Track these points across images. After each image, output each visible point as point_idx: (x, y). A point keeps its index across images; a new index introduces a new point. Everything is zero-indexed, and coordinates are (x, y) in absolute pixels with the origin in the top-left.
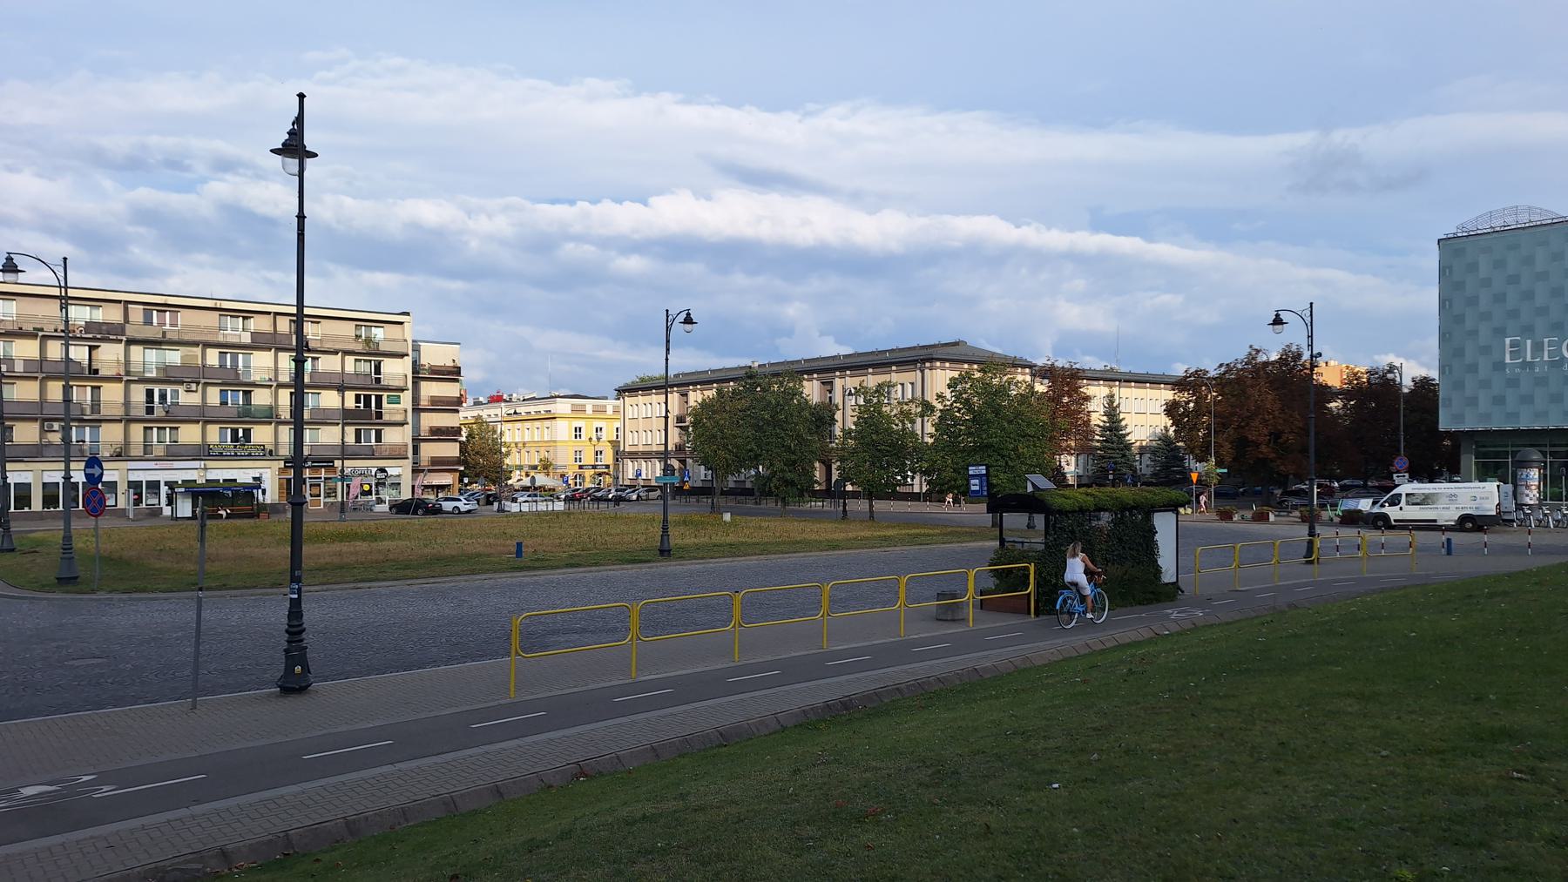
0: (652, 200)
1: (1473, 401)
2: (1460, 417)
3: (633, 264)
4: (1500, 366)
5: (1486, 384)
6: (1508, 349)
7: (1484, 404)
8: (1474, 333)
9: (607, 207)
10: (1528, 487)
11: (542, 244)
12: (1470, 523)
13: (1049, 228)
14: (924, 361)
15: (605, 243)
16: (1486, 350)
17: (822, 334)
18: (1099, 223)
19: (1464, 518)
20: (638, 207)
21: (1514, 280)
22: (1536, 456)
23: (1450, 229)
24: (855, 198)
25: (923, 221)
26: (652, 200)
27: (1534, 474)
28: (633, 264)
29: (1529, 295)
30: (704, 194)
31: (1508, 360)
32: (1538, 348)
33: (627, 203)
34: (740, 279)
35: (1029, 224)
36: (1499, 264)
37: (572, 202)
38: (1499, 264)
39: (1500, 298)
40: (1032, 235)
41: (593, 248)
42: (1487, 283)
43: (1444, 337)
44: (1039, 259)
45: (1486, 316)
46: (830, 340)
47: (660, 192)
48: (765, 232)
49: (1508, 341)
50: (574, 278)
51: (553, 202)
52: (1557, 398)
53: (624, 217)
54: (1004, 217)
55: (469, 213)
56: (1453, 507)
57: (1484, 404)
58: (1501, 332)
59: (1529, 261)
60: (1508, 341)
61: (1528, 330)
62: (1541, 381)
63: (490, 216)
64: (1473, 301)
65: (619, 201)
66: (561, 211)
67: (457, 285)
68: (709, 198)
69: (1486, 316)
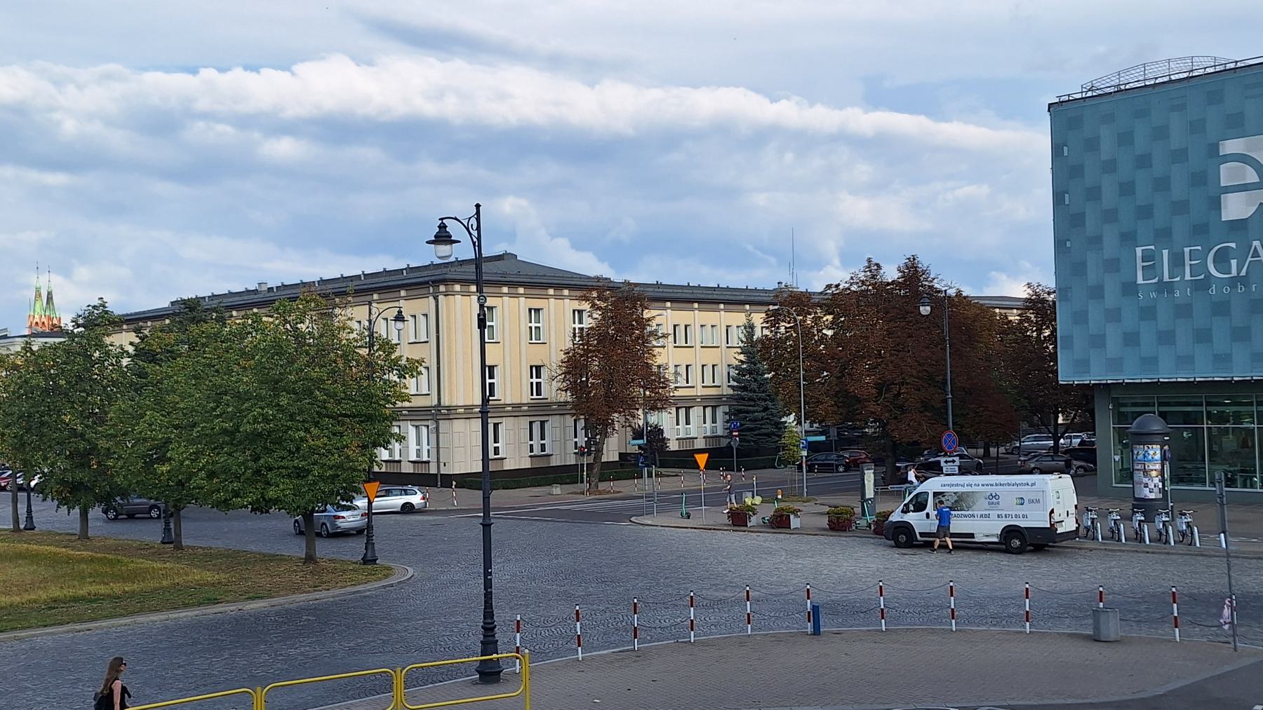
0: (297, 68)
1: (1098, 341)
2: (1083, 365)
3: (284, 148)
4: (1130, 288)
5: (1114, 315)
6: (1140, 264)
7: (1113, 344)
8: (1097, 241)
9: (238, 76)
10: (1146, 473)
11: (161, 123)
12: (1024, 541)
13: (811, 105)
14: (436, 283)
15: (245, 122)
16: (1112, 265)
17: (553, 236)
18: (877, 96)
19: (1010, 532)
20: (283, 76)
21: (1143, 161)
22: (1157, 426)
23: (1073, 87)
24: (555, 63)
25: (656, 93)
26: (295, 68)
27: (1155, 452)
28: (284, 148)
29: (1162, 184)
30: (363, 59)
31: (1140, 281)
32: (1177, 261)
33: (264, 71)
34: (430, 168)
35: (788, 98)
36: (1125, 139)
37: (193, 71)
38: (1125, 139)
39: (1127, 189)
40: (787, 112)
41: (229, 129)
42: (1110, 166)
43: (1060, 244)
44: (803, 141)
45: (1111, 216)
46: (563, 243)
47: (305, 57)
48: (450, 108)
49: (1139, 251)
50: (205, 169)
51: (167, 69)
52: (1241, 335)
53: (265, 89)
54: (757, 90)
55: (58, 83)
56: (994, 514)
57: (1113, 344)
58: (1129, 239)
59: (1161, 133)
60: (1139, 251)
61: (1163, 236)
62: (1183, 311)
63: (80, 87)
64: (1094, 194)
65: (253, 68)
66: (179, 82)
67: (56, 179)
68: (370, 63)
69: (1111, 216)
